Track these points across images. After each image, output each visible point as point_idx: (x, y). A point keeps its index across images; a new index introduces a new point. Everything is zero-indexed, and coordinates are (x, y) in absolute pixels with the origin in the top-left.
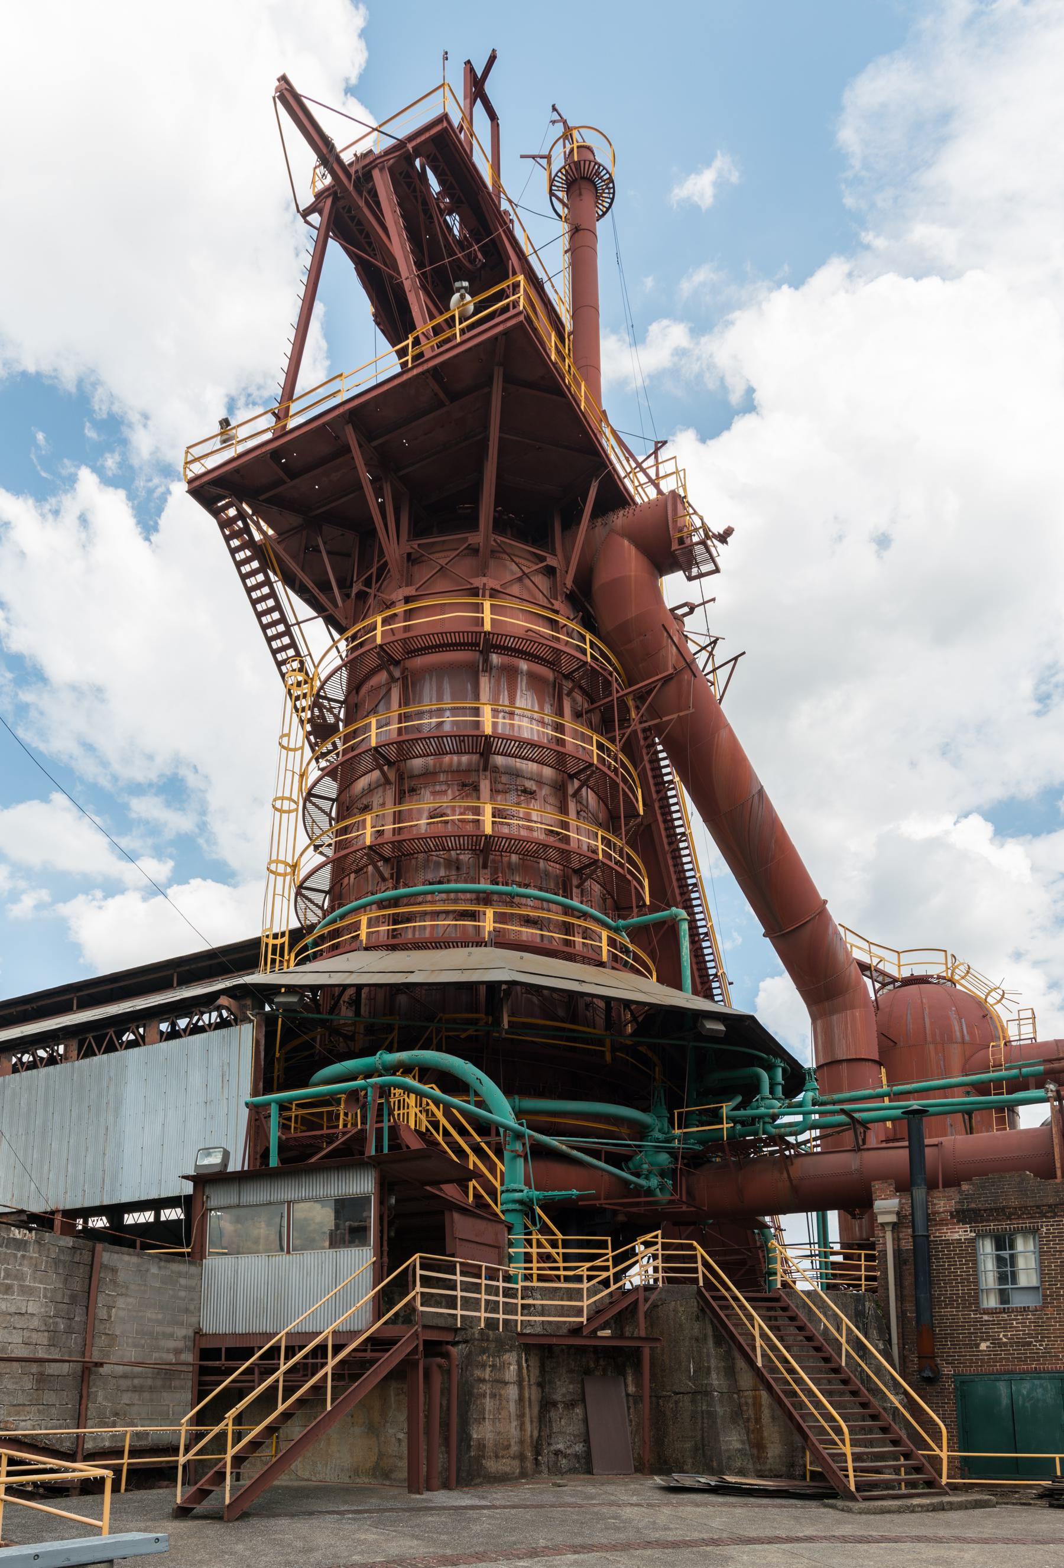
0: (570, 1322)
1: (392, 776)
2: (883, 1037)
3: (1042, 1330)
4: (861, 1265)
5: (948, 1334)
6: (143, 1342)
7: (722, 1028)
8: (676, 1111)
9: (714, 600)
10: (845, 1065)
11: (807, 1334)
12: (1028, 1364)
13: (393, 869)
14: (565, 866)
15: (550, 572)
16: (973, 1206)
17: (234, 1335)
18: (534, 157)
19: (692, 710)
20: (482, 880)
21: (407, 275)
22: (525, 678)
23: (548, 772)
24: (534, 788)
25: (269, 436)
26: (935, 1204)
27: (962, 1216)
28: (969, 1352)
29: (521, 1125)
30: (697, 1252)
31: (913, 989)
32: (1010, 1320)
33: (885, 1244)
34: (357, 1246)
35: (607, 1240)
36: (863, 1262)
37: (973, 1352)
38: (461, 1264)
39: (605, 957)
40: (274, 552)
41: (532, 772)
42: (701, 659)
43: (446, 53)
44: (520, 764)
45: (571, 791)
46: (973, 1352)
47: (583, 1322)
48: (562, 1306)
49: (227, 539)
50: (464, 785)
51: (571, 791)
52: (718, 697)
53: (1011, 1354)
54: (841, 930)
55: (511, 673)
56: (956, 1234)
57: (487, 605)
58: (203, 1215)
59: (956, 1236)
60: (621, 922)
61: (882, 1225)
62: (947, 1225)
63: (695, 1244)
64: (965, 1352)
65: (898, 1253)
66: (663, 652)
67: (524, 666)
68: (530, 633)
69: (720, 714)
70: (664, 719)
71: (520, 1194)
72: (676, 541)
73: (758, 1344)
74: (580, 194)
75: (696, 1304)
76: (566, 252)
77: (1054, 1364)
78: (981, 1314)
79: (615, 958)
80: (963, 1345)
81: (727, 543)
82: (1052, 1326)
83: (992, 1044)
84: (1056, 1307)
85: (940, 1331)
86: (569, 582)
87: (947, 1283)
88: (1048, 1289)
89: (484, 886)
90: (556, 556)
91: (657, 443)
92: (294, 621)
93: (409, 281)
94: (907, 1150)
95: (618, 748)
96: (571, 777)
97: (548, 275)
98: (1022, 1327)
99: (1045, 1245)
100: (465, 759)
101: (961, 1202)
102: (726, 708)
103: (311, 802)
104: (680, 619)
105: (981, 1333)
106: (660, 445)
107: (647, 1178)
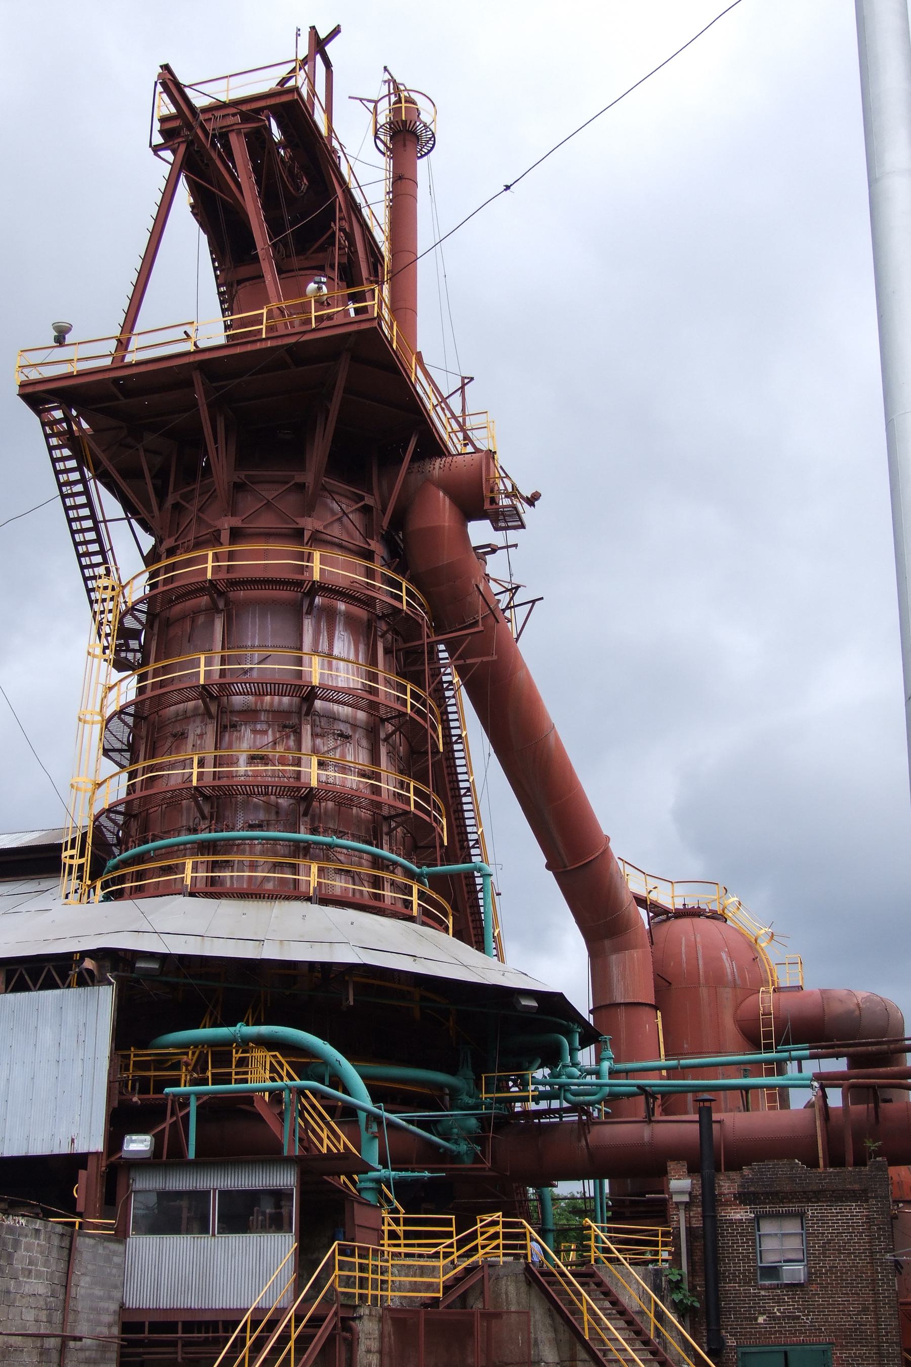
0: (421, 1297)
1: (213, 709)
2: (660, 979)
3: (808, 1305)
4: (658, 1241)
5: (731, 1308)
6: (92, 1317)
7: (535, 1004)
8: (483, 1076)
9: (516, 546)
10: (623, 1008)
11: (620, 1308)
12: (797, 1337)
13: (212, 808)
14: (375, 813)
15: (366, 510)
16: (752, 1189)
17: (158, 1310)
18: (361, 100)
19: (495, 657)
20: (302, 828)
21: (263, 246)
22: (342, 618)
23: (361, 715)
24: (350, 732)
25: (107, 362)
26: (722, 1186)
27: (744, 1198)
28: (749, 1325)
29: (380, 1108)
30: (527, 1230)
31: (686, 922)
32: (783, 1295)
33: (678, 1221)
34: (275, 1232)
35: (452, 1219)
36: (660, 1238)
37: (752, 1324)
38: (359, 1247)
39: (415, 912)
40: (89, 447)
41: (347, 716)
42: (504, 599)
43: (299, 30)
44: (336, 707)
45: (382, 735)
46: (752, 1324)
47: (439, 1297)
48: (416, 1282)
49: (47, 437)
50: (285, 727)
51: (382, 735)
52: (515, 636)
53: (783, 1327)
54: (620, 863)
55: (330, 615)
56: (738, 1215)
57: (317, 555)
58: (127, 1197)
59: (738, 1216)
60: (425, 869)
61: (677, 1203)
62: (730, 1205)
63: (524, 1221)
64: (746, 1325)
65: (689, 1230)
66: (469, 599)
67: (342, 606)
68: (355, 584)
69: (517, 651)
70: (468, 661)
71: (378, 1173)
72: (489, 500)
73: (585, 1319)
74: (405, 145)
75: (524, 1279)
76: (388, 193)
77: (818, 1336)
78: (758, 1289)
79: (426, 912)
80: (744, 1318)
81: (534, 506)
82: (816, 1301)
83: (762, 989)
84: (818, 1284)
85: (725, 1304)
86: (385, 523)
87: (730, 1260)
88: (813, 1267)
89: (303, 835)
90: (373, 495)
91: (463, 378)
92: (101, 519)
93: (264, 251)
94: (697, 1126)
95: (427, 694)
96: (383, 721)
97: (366, 202)
98: (793, 1302)
99: (811, 1227)
100: (286, 699)
101: (742, 1186)
102: (523, 647)
103: (119, 718)
104: (482, 558)
105: (759, 1307)
106: (466, 381)
107: (456, 1142)
